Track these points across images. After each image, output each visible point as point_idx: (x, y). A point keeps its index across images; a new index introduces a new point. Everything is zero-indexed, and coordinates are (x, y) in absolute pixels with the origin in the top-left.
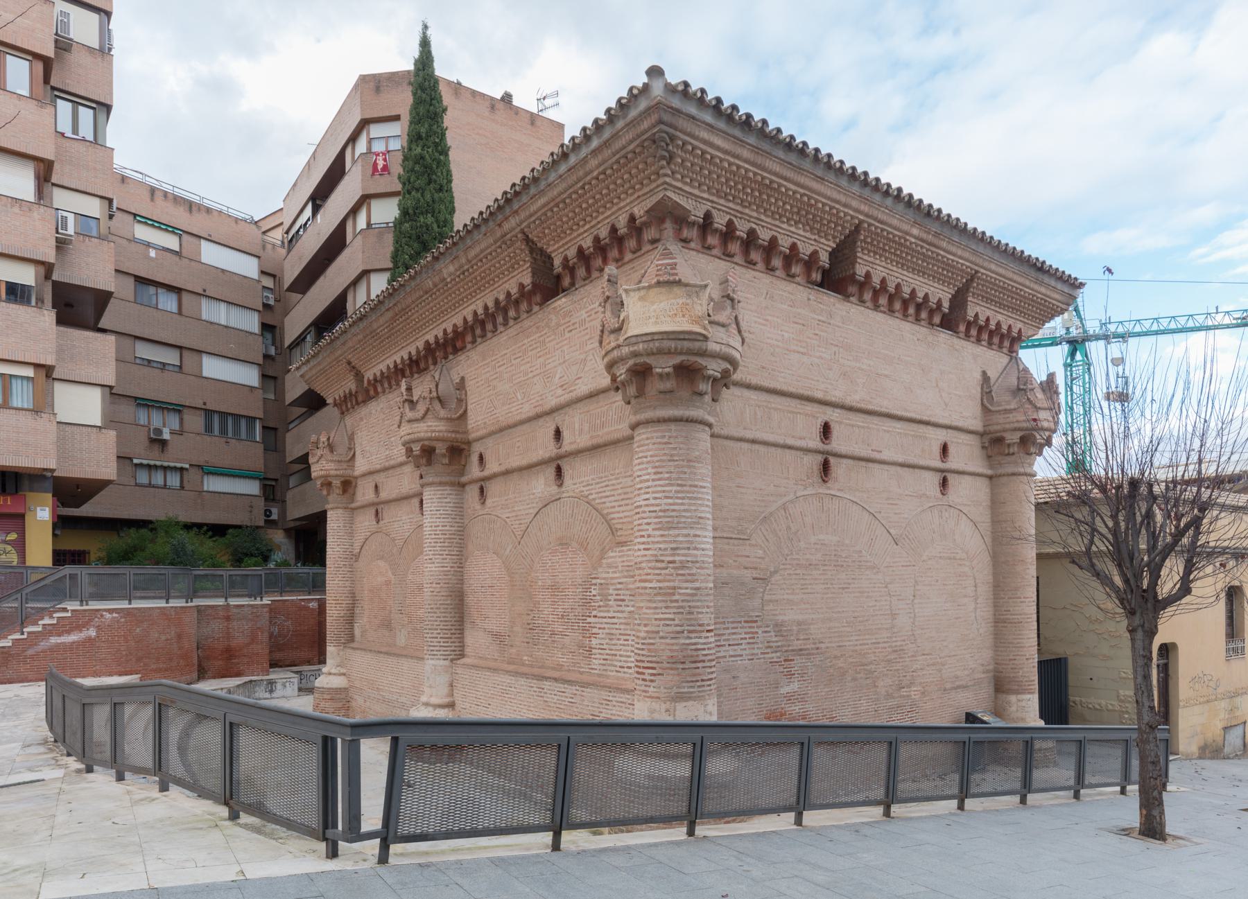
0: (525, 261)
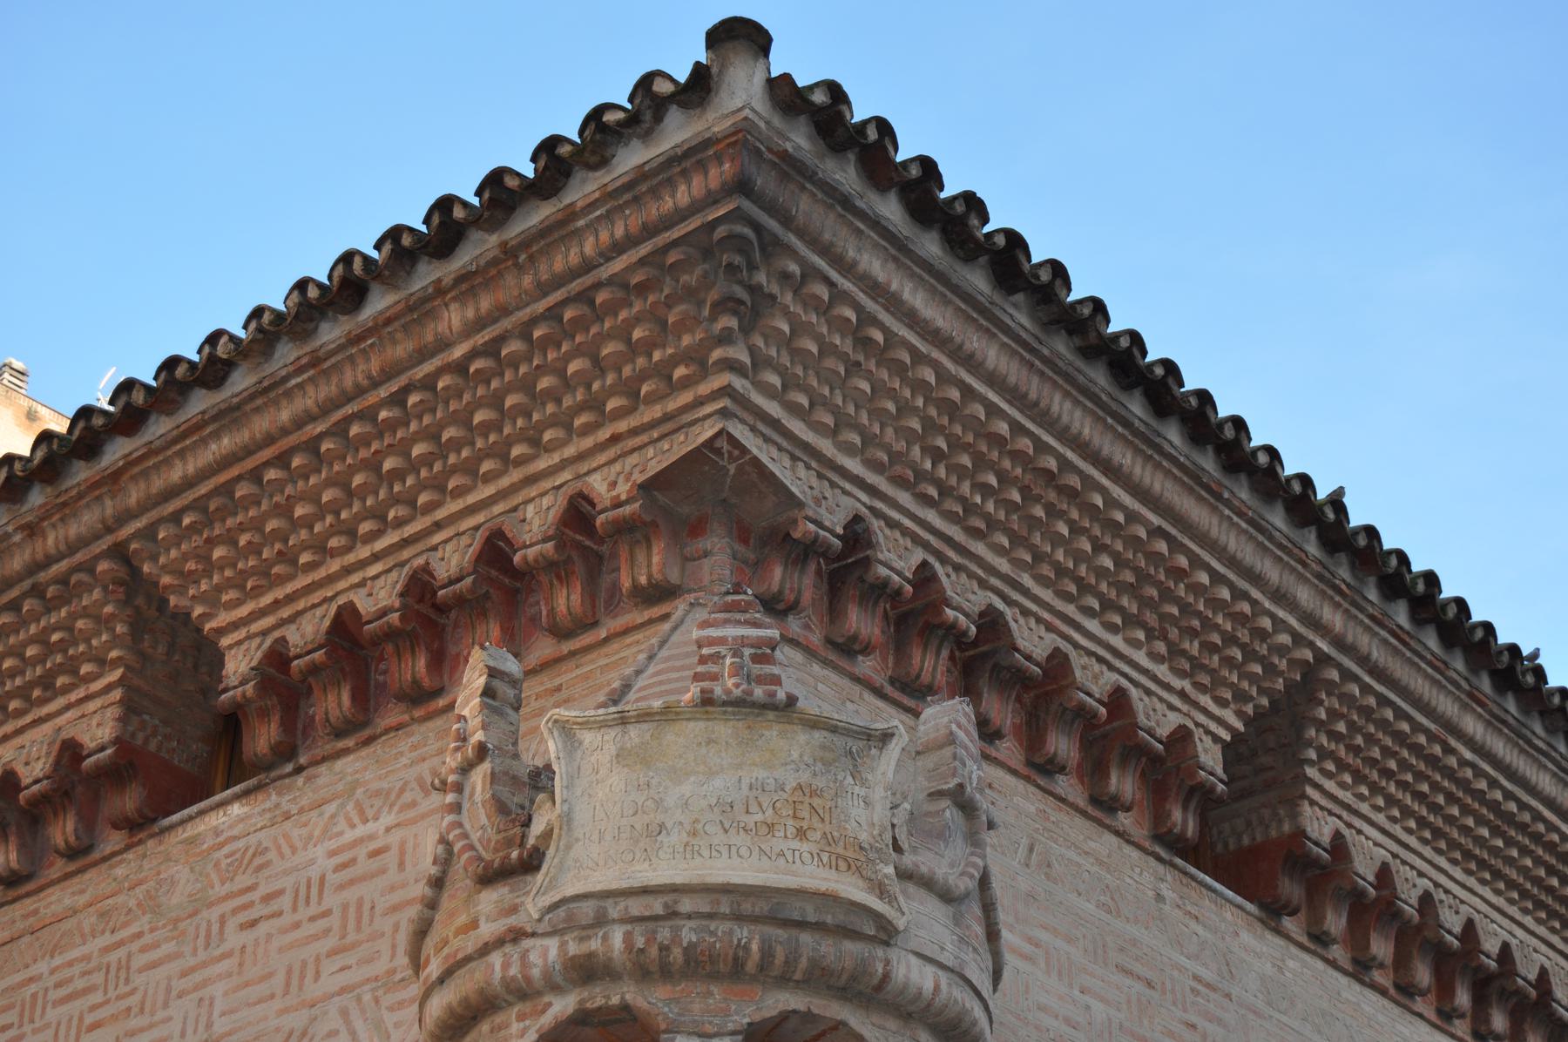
0: (102, 662)
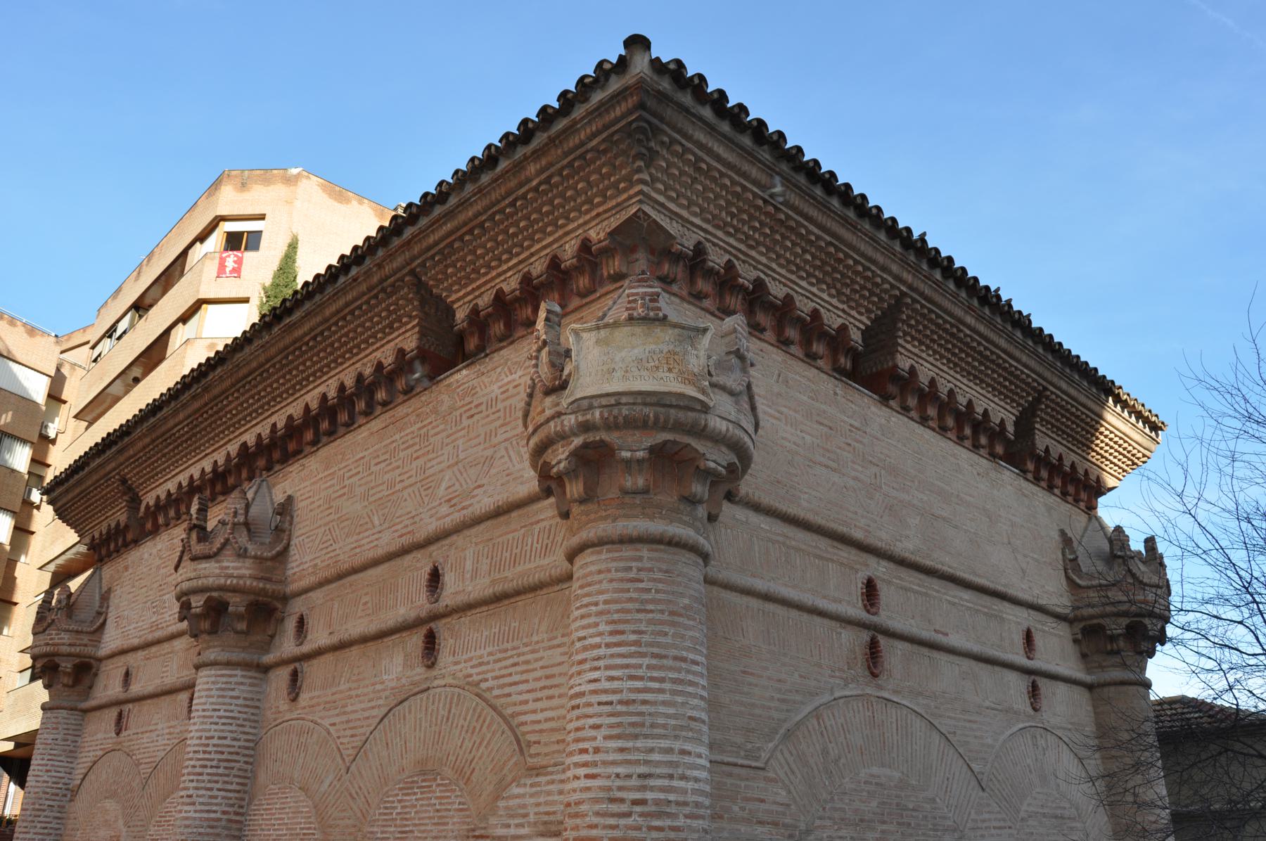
0: (410, 317)
